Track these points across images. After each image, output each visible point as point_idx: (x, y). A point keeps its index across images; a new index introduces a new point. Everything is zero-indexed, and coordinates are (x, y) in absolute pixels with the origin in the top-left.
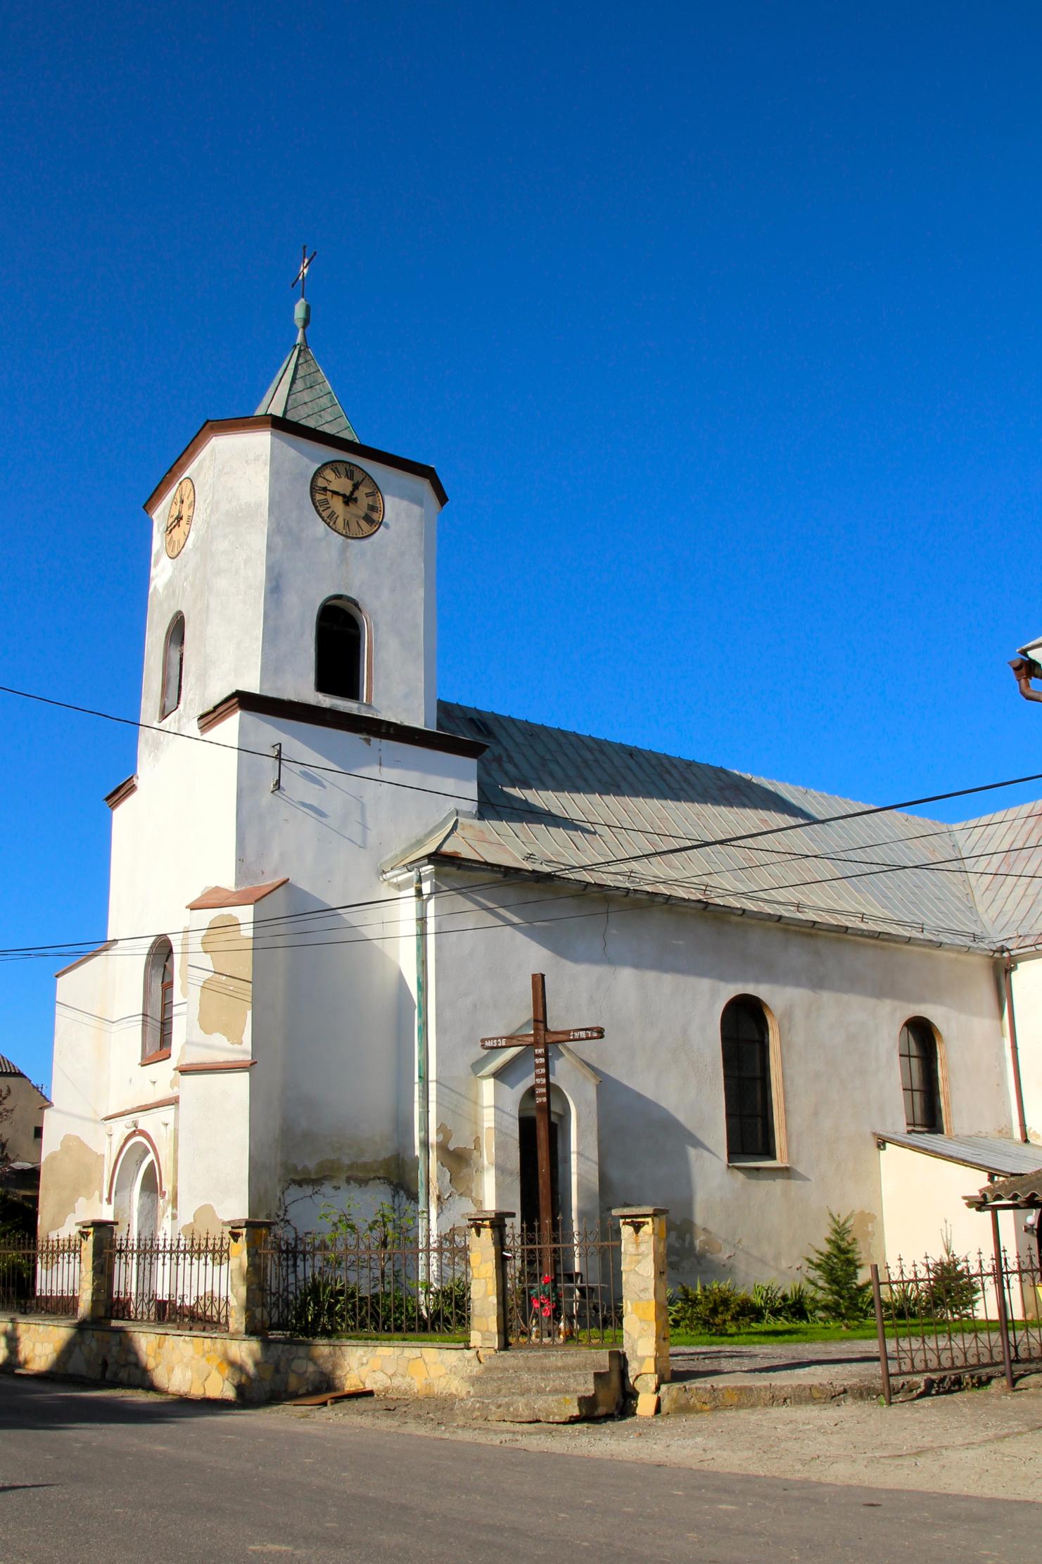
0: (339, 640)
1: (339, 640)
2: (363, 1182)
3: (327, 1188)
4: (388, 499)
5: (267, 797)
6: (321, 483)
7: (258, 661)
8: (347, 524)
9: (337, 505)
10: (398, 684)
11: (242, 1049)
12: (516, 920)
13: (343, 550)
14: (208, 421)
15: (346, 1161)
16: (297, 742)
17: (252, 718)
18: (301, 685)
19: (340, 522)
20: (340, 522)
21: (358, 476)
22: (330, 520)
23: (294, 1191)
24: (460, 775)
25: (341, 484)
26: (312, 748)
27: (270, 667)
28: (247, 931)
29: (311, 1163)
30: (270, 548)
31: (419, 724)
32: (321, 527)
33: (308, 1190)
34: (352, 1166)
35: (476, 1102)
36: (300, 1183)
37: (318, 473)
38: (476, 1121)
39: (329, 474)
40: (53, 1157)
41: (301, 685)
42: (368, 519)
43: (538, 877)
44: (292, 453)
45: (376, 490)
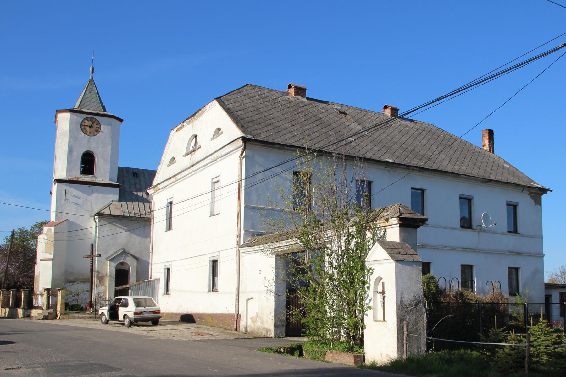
0: (88, 162)
1: (88, 162)
2: (84, 282)
3: (76, 284)
4: (102, 126)
5: (63, 202)
6: (83, 124)
7: (66, 169)
8: (90, 133)
9: (88, 128)
10: (104, 172)
11: (52, 257)
12: (120, 226)
13: (89, 140)
14: (247, 85)
15: (81, 278)
16: (72, 190)
17: (60, 184)
18: (77, 175)
19: (88, 133)
20: (88, 133)
21: (94, 120)
22: (85, 133)
23: (68, 284)
24: (114, 194)
25: (88, 123)
26: (154, 179)
27: (69, 170)
28: (53, 232)
29: (72, 279)
30: (69, 142)
31: (107, 181)
32: (83, 134)
33: (71, 284)
34: (82, 279)
35: (107, 265)
36: (69, 282)
37: (83, 121)
38: (106, 270)
39: (86, 121)
40: (37, 276)
41: (77, 175)
42: (97, 131)
43: (124, 217)
44: (76, 117)
45: (99, 124)
